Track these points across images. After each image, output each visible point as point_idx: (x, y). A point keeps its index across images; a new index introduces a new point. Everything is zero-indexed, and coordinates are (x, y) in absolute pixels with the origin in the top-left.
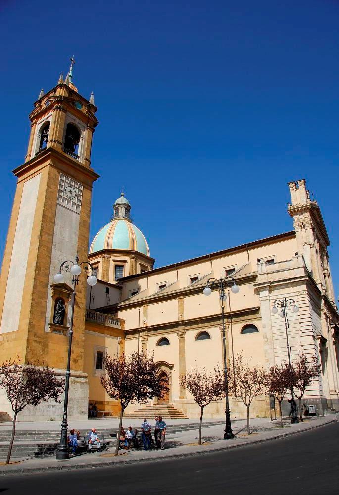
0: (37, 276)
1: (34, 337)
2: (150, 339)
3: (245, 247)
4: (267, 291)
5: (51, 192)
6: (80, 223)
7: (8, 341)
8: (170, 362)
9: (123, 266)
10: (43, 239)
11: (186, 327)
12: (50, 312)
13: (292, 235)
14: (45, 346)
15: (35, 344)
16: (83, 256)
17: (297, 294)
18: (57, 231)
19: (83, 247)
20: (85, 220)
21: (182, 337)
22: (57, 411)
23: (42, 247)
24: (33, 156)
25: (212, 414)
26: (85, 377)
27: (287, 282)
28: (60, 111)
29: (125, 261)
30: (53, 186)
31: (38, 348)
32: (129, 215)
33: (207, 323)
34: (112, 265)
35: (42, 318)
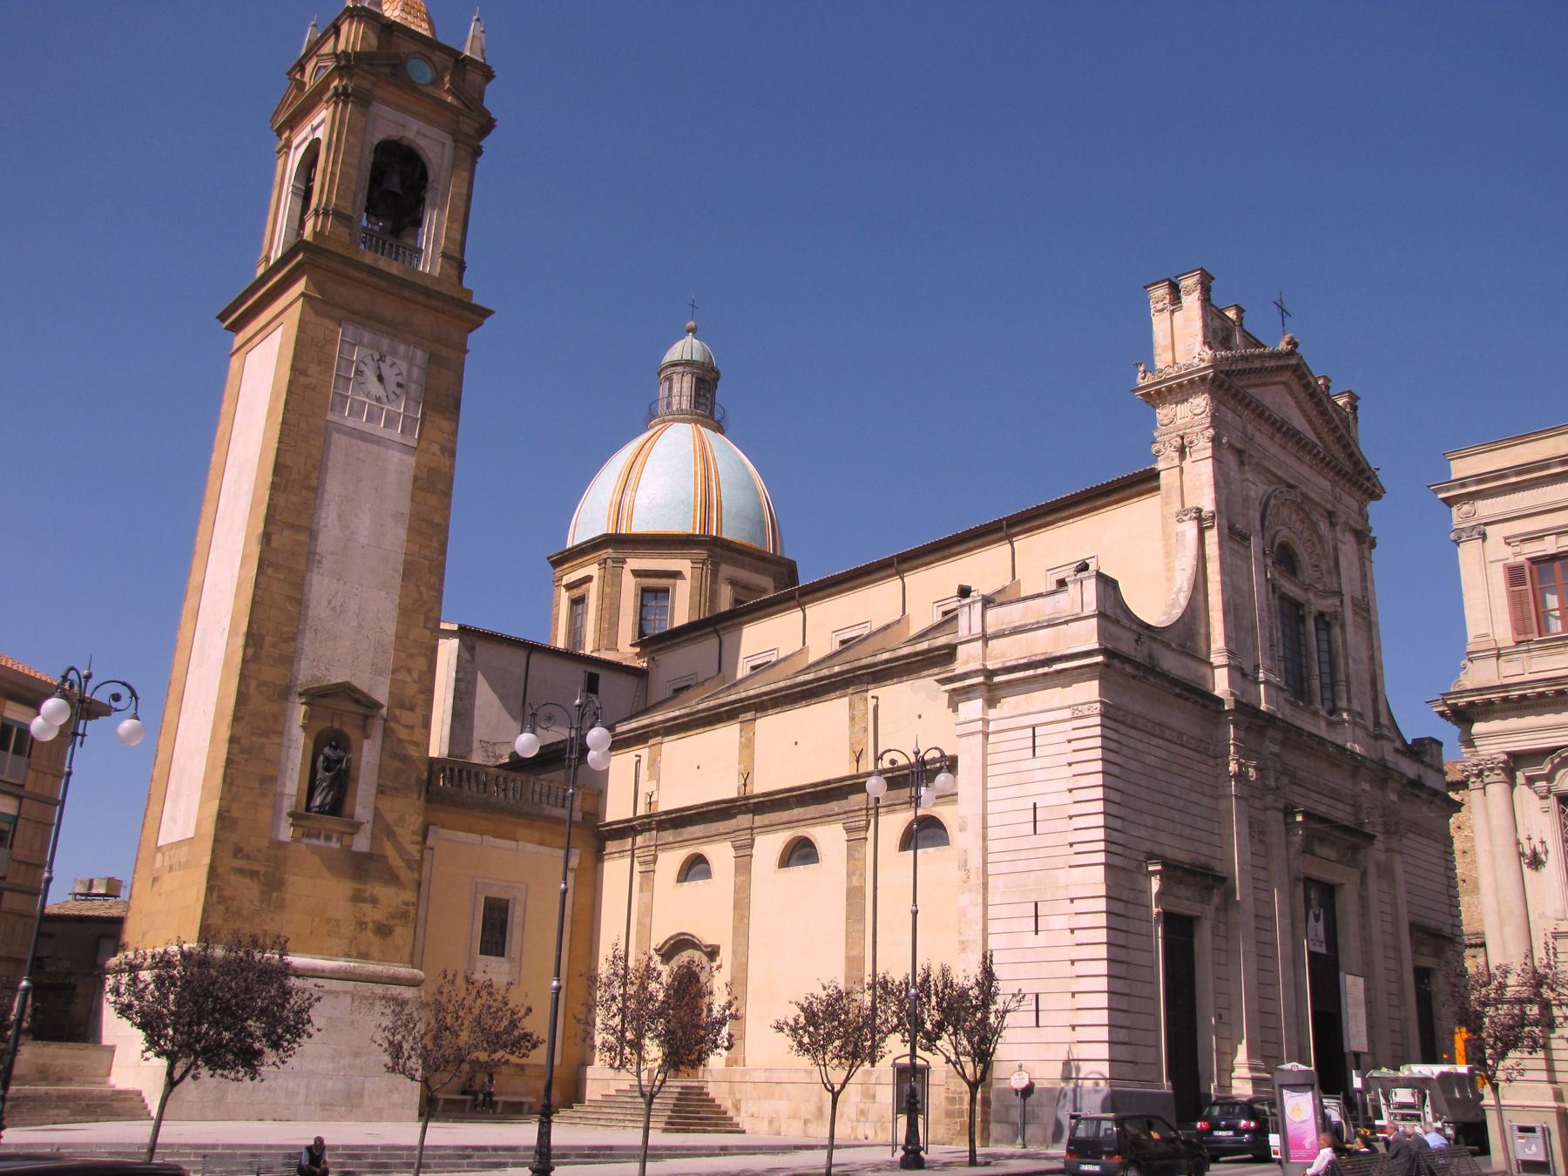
0: (253, 666)
1: (235, 856)
2: (759, 840)
3: (1000, 529)
4: (980, 701)
5: (307, 386)
6: (416, 479)
7: (171, 869)
8: (708, 939)
9: (666, 590)
10: (274, 544)
11: (760, 820)
12: (296, 777)
13: (1144, 482)
14: (273, 884)
15: (235, 880)
16: (423, 589)
17: (1067, 714)
18: (329, 517)
19: (425, 557)
20: (433, 465)
21: (744, 852)
22: (303, 1091)
23: (270, 571)
24: (277, 253)
25: (806, 1122)
26: (413, 983)
27: (1040, 671)
28: (345, 104)
29: (676, 575)
30: (313, 369)
31: (247, 892)
32: (707, 402)
33: (801, 810)
34: (629, 585)
35: (264, 795)
